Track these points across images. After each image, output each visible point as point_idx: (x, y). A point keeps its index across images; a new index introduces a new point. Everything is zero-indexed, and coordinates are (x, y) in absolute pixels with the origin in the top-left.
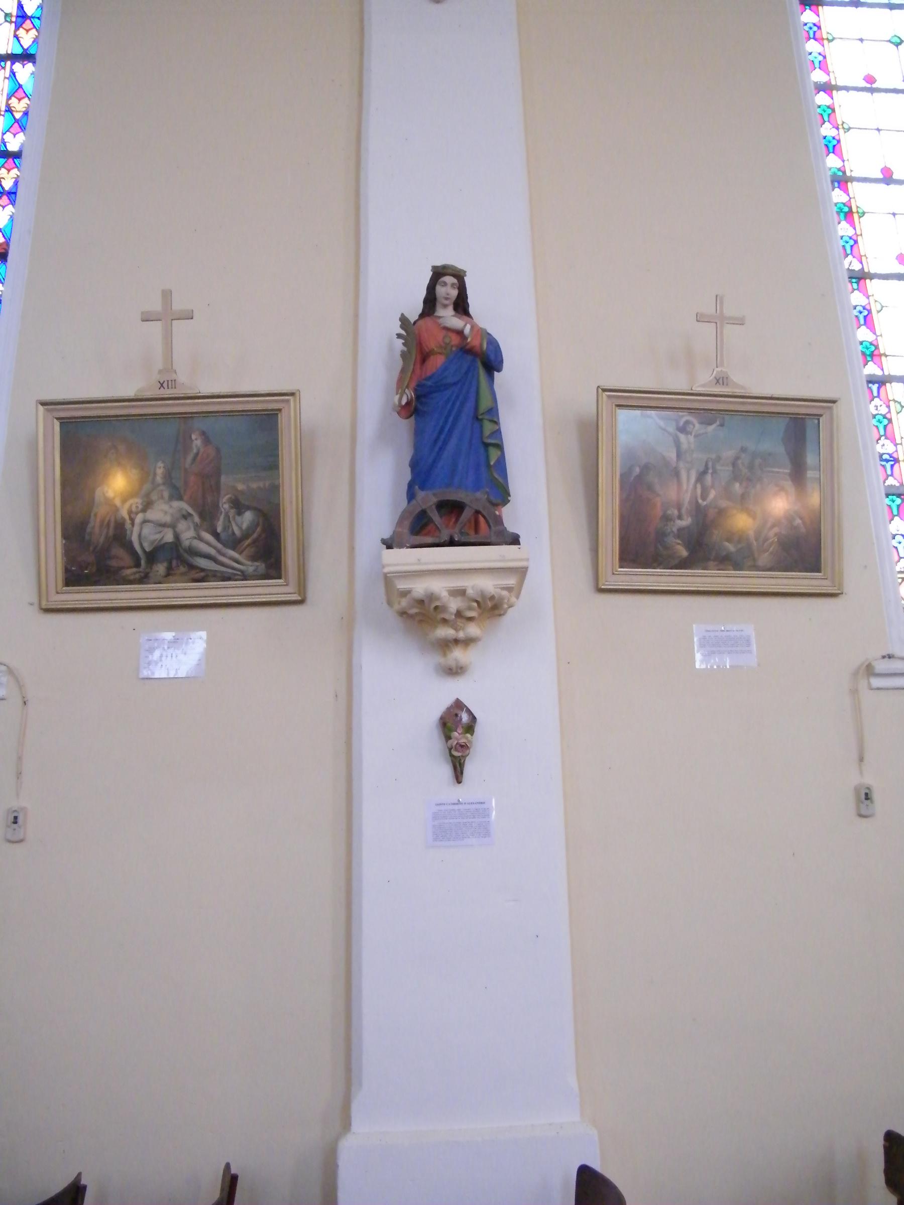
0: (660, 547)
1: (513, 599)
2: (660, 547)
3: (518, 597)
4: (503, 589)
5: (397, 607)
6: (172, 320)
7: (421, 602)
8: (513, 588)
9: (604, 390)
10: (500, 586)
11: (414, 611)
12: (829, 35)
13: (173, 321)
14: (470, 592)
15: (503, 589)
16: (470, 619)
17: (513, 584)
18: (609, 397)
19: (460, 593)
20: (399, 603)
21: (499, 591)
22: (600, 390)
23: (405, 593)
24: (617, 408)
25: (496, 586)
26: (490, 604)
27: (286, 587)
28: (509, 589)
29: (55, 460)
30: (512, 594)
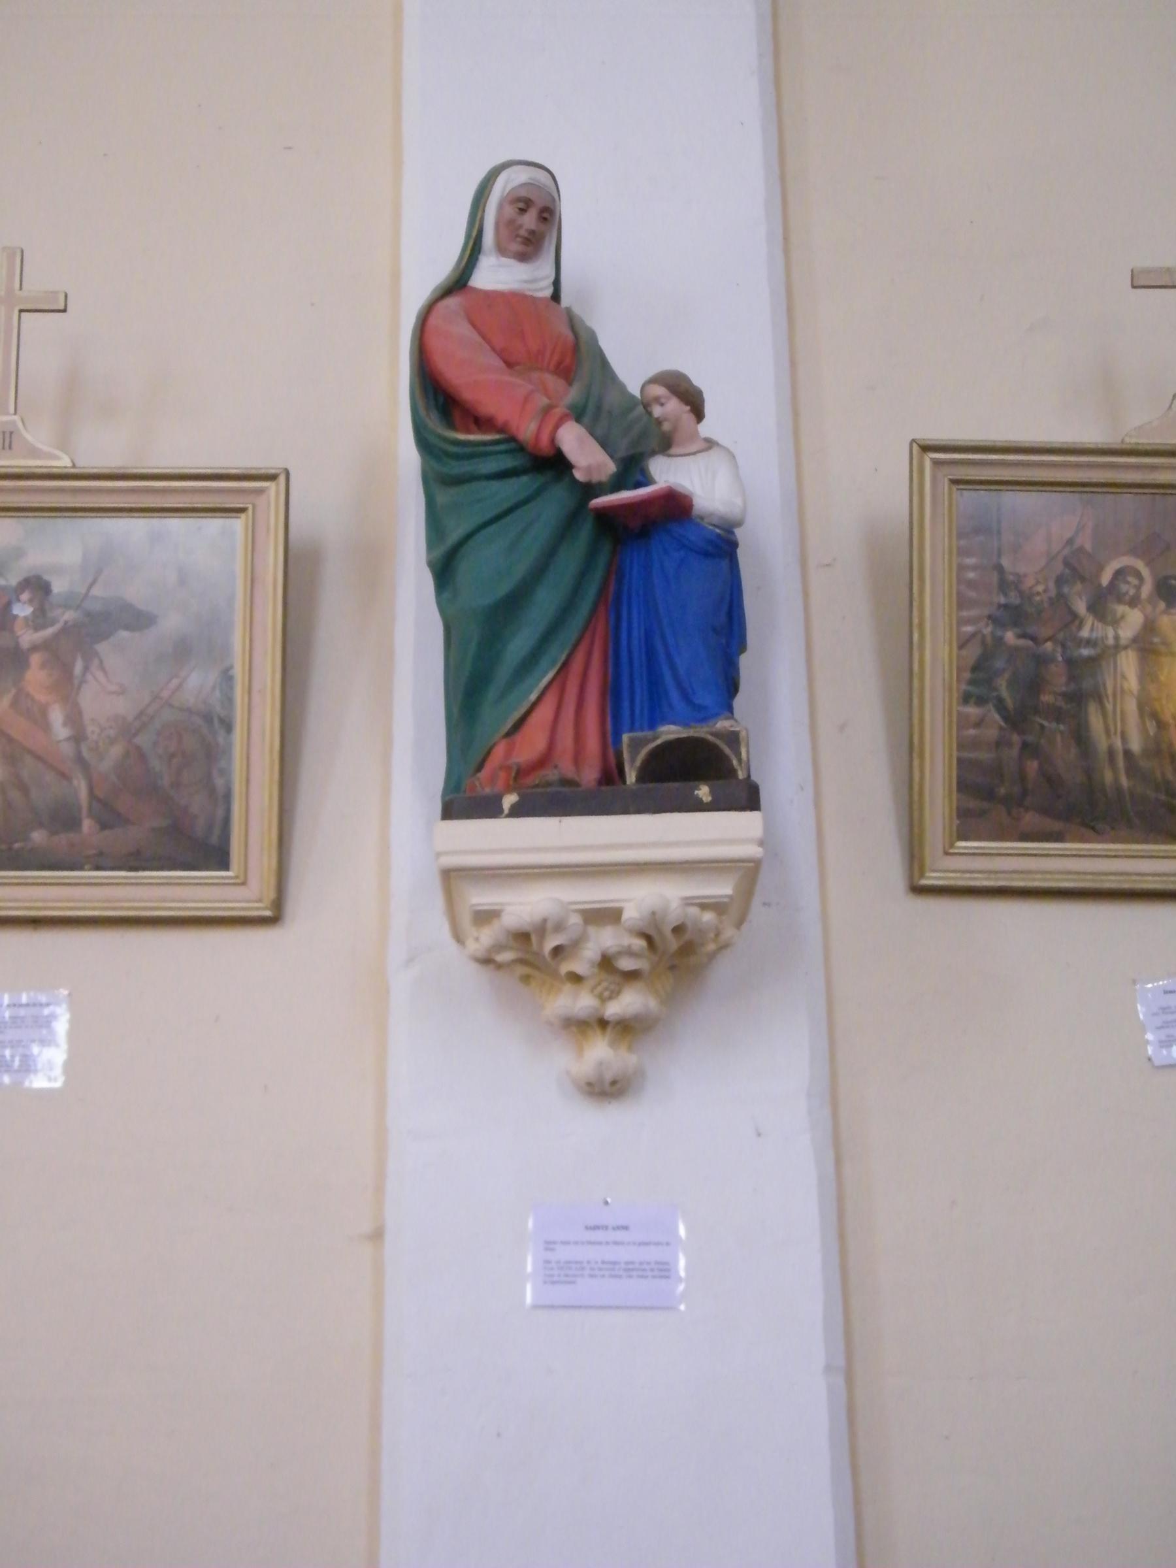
0: (497, 437)
1: (729, 932)
2: (497, 437)
3: (739, 923)
4: (704, 907)
5: (472, 947)
6: (21, 311)
7: (522, 937)
8: (725, 904)
9: (926, 448)
10: (698, 901)
11: (505, 957)
12: (703, 445)
13: (23, 314)
14: (631, 914)
15: (704, 907)
16: (632, 976)
17: (726, 896)
18: (937, 463)
19: (609, 916)
20: (477, 939)
21: (694, 911)
22: (915, 446)
23: (485, 917)
24: (954, 488)
25: (688, 902)
26: (674, 944)
27: (242, 888)
28: (718, 907)
29: (1129, 481)
30: (724, 917)
